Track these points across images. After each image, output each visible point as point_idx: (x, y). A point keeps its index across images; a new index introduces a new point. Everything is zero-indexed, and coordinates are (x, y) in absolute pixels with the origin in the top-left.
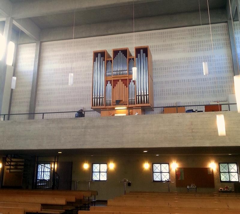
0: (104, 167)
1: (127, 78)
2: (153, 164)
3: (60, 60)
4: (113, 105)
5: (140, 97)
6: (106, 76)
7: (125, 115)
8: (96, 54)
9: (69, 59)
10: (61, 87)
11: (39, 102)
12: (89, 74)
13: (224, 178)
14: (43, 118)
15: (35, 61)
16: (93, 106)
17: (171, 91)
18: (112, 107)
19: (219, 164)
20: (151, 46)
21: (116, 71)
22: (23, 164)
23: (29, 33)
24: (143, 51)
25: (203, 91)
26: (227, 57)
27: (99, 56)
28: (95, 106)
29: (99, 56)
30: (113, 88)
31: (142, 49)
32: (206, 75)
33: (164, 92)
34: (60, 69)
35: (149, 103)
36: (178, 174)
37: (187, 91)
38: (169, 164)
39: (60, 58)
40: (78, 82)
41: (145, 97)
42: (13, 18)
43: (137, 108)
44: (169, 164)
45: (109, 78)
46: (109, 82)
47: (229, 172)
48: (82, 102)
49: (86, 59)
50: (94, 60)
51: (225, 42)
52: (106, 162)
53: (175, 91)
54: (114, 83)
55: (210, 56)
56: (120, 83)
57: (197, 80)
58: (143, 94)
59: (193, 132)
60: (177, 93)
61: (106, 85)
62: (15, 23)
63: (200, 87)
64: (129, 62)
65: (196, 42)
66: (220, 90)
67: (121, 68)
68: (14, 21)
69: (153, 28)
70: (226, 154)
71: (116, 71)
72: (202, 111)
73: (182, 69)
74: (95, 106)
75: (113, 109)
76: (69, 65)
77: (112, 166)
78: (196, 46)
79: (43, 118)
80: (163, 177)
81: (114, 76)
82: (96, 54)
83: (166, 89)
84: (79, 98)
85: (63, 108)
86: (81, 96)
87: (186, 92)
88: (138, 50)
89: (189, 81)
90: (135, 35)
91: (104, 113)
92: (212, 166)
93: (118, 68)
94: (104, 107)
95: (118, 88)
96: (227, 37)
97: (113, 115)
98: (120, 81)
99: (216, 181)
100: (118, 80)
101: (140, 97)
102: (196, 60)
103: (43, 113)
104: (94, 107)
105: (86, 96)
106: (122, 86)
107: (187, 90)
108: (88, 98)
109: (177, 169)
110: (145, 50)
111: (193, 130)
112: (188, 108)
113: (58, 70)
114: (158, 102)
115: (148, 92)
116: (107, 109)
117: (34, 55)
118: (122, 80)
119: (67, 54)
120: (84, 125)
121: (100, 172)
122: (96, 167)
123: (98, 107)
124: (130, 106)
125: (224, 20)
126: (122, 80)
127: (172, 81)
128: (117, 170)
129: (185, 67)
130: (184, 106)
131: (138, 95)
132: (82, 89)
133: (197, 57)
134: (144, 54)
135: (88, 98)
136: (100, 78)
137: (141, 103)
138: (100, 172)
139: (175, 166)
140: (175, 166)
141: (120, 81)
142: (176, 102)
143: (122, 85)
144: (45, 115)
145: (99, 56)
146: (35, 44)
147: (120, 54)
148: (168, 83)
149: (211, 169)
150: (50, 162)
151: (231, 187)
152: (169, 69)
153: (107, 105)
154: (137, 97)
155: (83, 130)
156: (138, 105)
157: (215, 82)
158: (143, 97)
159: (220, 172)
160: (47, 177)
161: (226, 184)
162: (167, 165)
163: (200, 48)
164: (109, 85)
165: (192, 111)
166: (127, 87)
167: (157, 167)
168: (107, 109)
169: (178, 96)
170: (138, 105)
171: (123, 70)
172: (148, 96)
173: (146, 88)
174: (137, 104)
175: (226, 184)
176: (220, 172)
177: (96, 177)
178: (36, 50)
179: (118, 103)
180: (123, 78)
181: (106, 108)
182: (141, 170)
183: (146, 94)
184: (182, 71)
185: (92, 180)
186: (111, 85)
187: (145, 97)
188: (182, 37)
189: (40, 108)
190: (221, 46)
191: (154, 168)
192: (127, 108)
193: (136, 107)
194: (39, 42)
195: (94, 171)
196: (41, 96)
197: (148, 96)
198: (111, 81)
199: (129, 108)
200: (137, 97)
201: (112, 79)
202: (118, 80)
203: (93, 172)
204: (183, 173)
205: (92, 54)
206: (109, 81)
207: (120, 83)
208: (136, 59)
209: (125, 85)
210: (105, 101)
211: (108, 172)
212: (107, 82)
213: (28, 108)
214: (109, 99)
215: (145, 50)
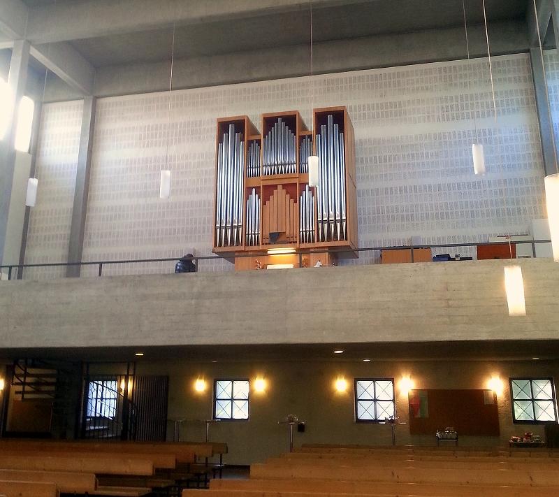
0: (241, 388)
1: (297, 181)
2: (356, 380)
3: (140, 139)
4: (263, 244)
5: (326, 225)
6: (246, 175)
7: (291, 266)
8: (223, 126)
9: (160, 137)
10: (142, 201)
11: (90, 238)
12: (206, 172)
13: (521, 413)
14: (100, 274)
15: (81, 143)
16: (216, 245)
17: (397, 211)
18: (261, 247)
19: (511, 380)
20: (351, 107)
21: (269, 164)
22: (54, 380)
23: (68, 76)
24: (334, 119)
25: (472, 212)
26: (529, 133)
27: (232, 130)
28: (220, 245)
29: (232, 129)
30: (264, 204)
31: (330, 113)
32: (480, 173)
33: (381, 215)
34: (139, 160)
35: (346, 239)
36: (416, 403)
37: (435, 212)
38: (392, 380)
39: (141, 135)
40: (181, 190)
41: (339, 225)
42: (29, 43)
43: (319, 250)
44: (392, 380)
45: (254, 182)
46: (254, 190)
47: (533, 400)
48: (191, 237)
49: (199, 138)
50: (220, 140)
51: (524, 97)
52: (246, 377)
53: (407, 211)
54: (266, 192)
55: (489, 130)
56: (280, 194)
57: (459, 185)
58: (333, 219)
59: (449, 306)
60: (412, 215)
61: (248, 198)
62: (35, 53)
63: (466, 202)
64: (300, 145)
65: (457, 97)
66: (513, 210)
67: (281, 159)
68: (32, 48)
69: (358, 65)
70: (527, 359)
71: (269, 164)
72: (471, 259)
73: (425, 160)
74: (220, 245)
75: (264, 253)
76: (160, 152)
77: (261, 385)
78: (457, 106)
79: (100, 274)
80: (379, 410)
81: (267, 177)
82: (223, 126)
83: (387, 207)
84: (183, 228)
85: (148, 250)
86: (188, 223)
87: (432, 214)
88: (321, 117)
89: (439, 187)
90: (315, 82)
91: (243, 262)
92: (495, 385)
93: (274, 159)
94: (242, 248)
95: (275, 205)
96: (529, 86)
97: (264, 267)
98: (280, 187)
99: (503, 421)
100: (275, 187)
101: (326, 225)
102: (457, 139)
103: (101, 264)
104: (219, 249)
105: (200, 223)
106: (284, 201)
107: (436, 209)
108: (204, 228)
109: (412, 393)
110: (339, 117)
111: (450, 302)
112: (437, 252)
113: (135, 163)
114: (367, 237)
115: (344, 213)
116: (250, 253)
117: (79, 129)
118: (284, 186)
119: (157, 125)
120: (195, 290)
121: (232, 400)
122: (224, 388)
123: (229, 249)
124: (304, 246)
125: (522, 47)
126: (284, 186)
127: (401, 188)
128: (274, 394)
129: (432, 155)
130: (429, 247)
131: (322, 222)
132: (192, 206)
133: (459, 133)
134: (336, 126)
135: (204, 228)
136: (233, 182)
137: (329, 238)
138: (232, 400)
139: (408, 385)
140: (408, 385)
141: (280, 187)
142: (409, 237)
143: (284, 196)
144: (105, 268)
145: (232, 129)
146: (82, 102)
147: (280, 125)
148: (392, 193)
149: (491, 393)
150: (116, 375)
151: (537, 435)
152: (395, 159)
153: (248, 244)
154: (320, 225)
155: (193, 302)
156: (322, 244)
157: (501, 191)
158: (333, 225)
159: (513, 400)
160: (109, 411)
161: (527, 428)
162: (389, 383)
163: (465, 111)
164: (254, 197)
165: (447, 257)
166: (295, 202)
167: (366, 388)
168: (250, 253)
169: (415, 222)
170: (322, 244)
171: (287, 162)
172: (344, 223)
173: (339, 205)
174: (318, 241)
175: (527, 428)
176: (513, 400)
177: (223, 412)
178: (84, 116)
179: (276, 238)
180: (286, 182)
181: (248, 251)
182: (328, 395)
183: (339, 218)
184: (423, 164)
185: (215, 418)
186: (259, 198)
187: (339, 225)
188: (423, 85)
189: (92, 252)
190: (516, 107)
191: (360, 390)
192: (295, 251)
193: (317, 250)
194: (92, 97)
195: (219, 398)
196: (96, 224)
197: (344, 223)
198: (258, 188)
199: (300, 252)
200: (320, 225)
201: (262, 184)
202: (275, 187)
203: (215, 399)
204: (426, 403)
205: (215, 126)
206: (254, 187)
207: (280, 194)
208: (316, 138)
209: (291, 198)
210: (245, 235)
211: (252, 400)
212: (248, 191)
213: (66, 252)
214: (255, 230)
215: (339, 117)
